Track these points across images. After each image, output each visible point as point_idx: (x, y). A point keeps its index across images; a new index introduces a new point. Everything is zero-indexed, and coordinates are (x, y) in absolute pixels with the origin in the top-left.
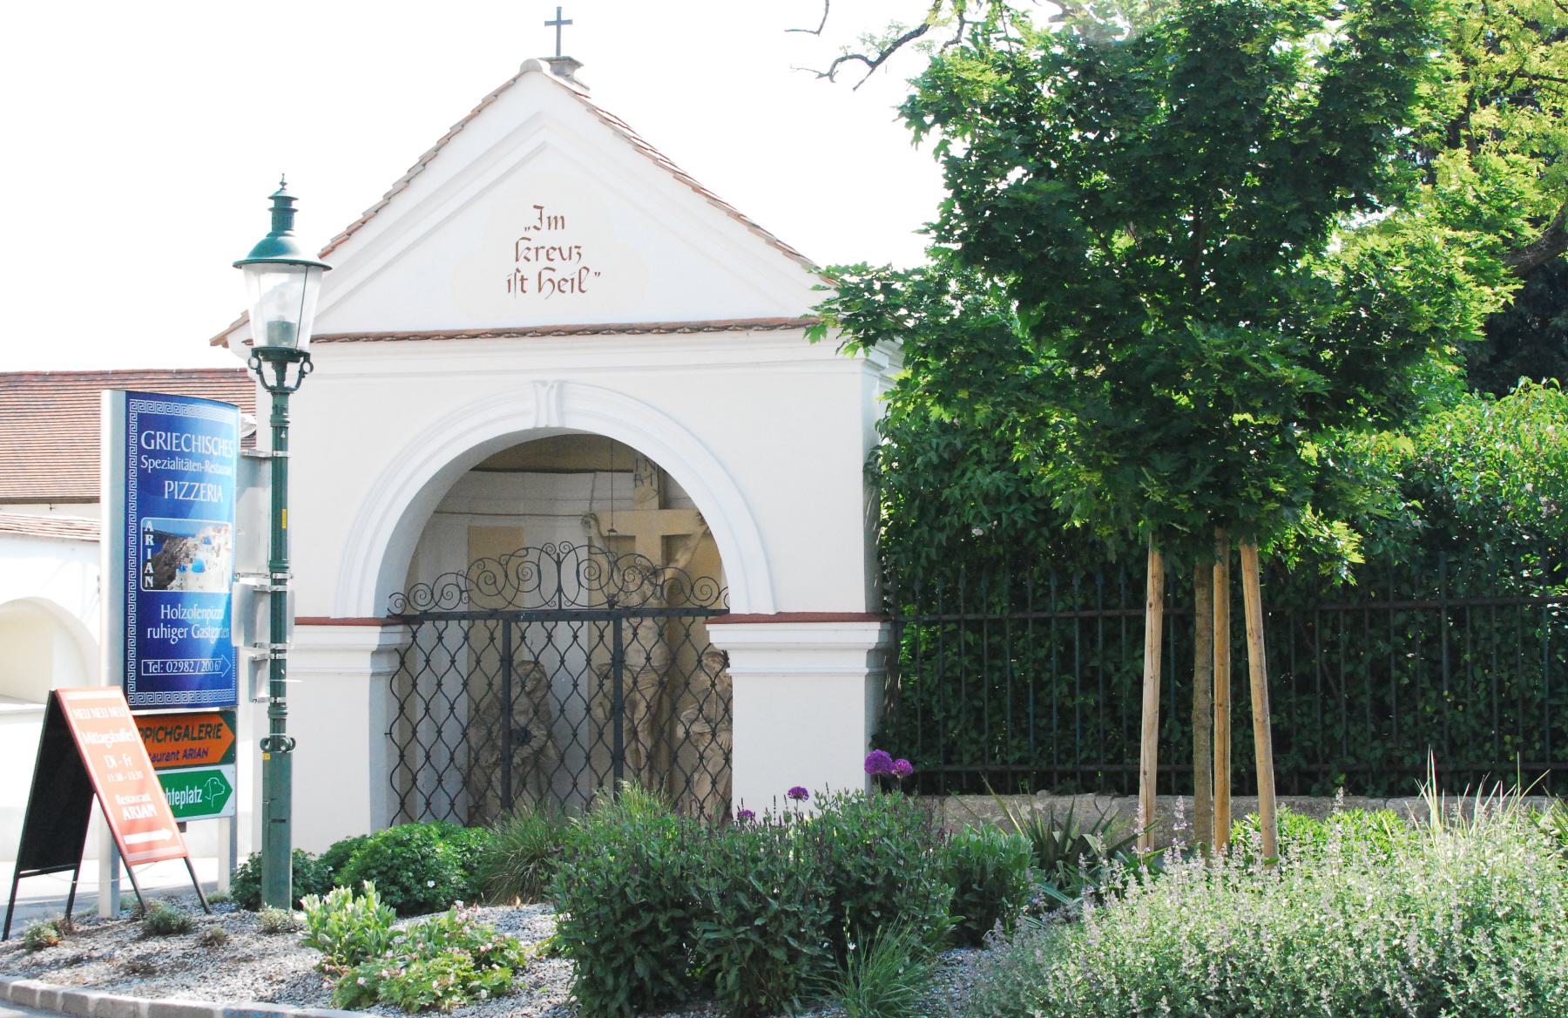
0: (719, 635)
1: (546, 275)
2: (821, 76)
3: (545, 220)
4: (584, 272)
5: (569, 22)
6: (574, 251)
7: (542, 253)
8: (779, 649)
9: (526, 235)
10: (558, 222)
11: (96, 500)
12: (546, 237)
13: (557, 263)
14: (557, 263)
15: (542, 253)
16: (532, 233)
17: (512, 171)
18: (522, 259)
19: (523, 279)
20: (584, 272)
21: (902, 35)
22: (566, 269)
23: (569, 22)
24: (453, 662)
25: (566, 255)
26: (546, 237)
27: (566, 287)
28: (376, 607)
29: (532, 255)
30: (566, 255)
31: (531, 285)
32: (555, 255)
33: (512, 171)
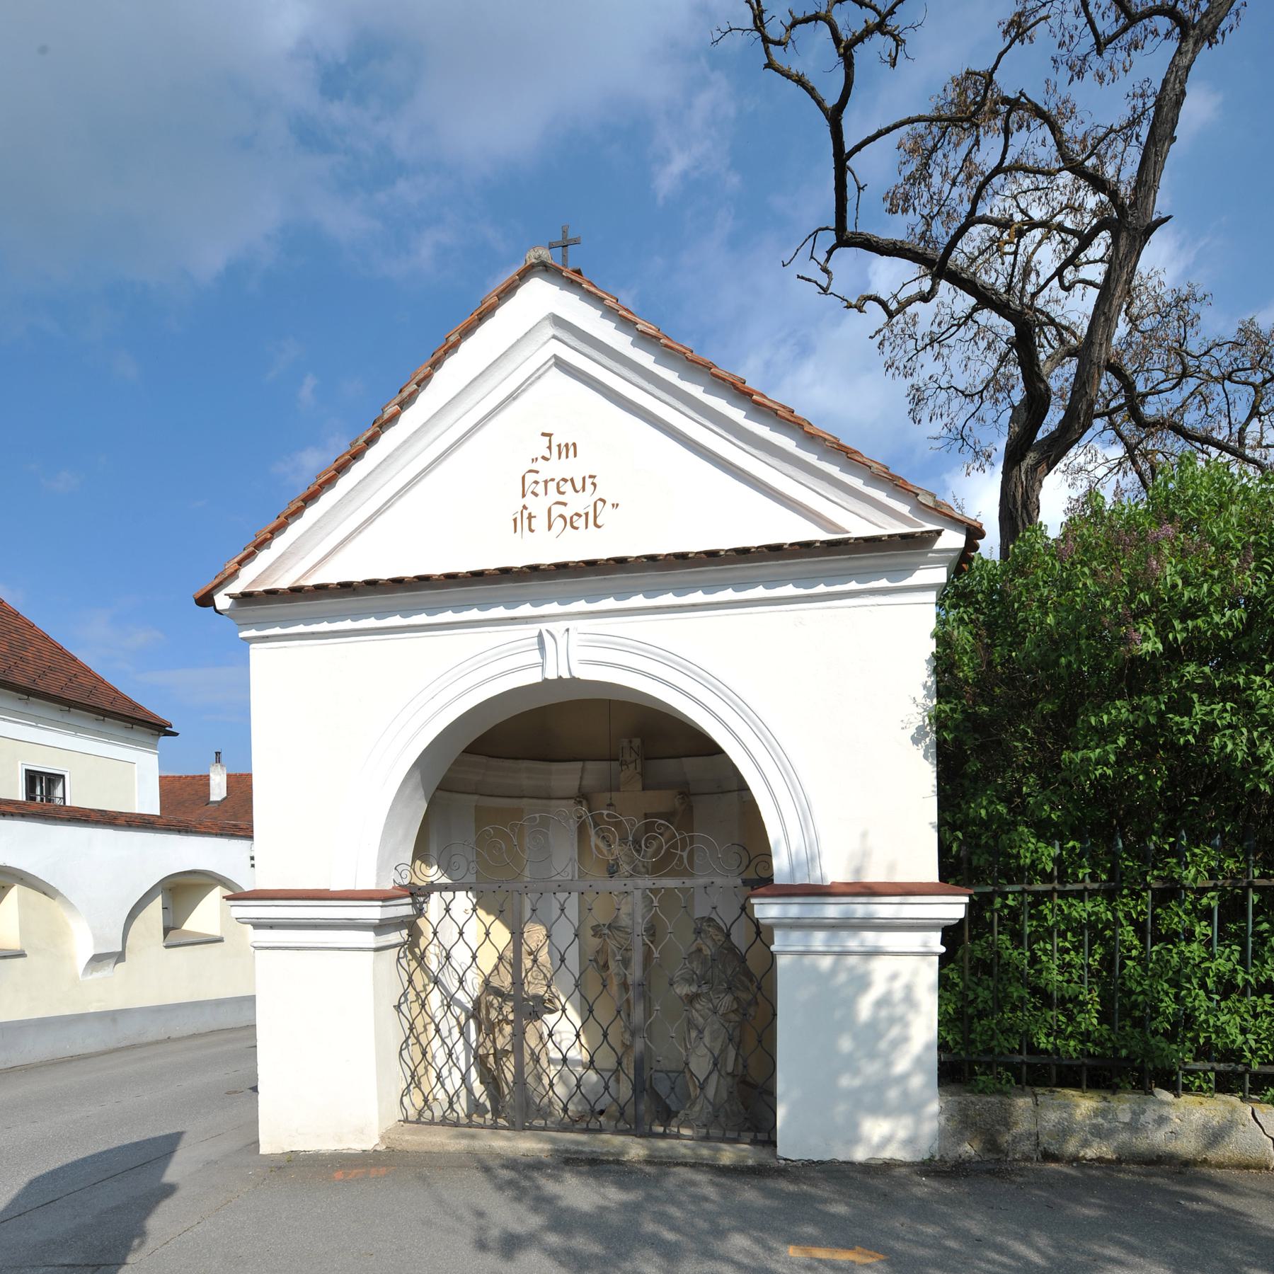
0: (768, 910)
1: (557, 510)
2: (849, 306)
3: (555, 449)
4: (600, 504)
5: (576, 242)
6: (588, 481)
7: (552, 486)
8: (494, 678)
9: (534, 467)
10: (568, 449)
11: (540, 635)
12: (557, 468)
13: (570, 496)
14: (570, 496)
15: (552, 486)
16: (540, 465)
17: (512, 397)
18: (529, 495)
19: (530, 517)
20: (600, 504)
21: (956, 225)
22: (579, 503)
23: (576, 242)
24: (461, 934)
25: (579, 486)
26: (557, 468)
27: (580, 522)
28: (380, 869)
29: (540, 489)
30: (579, 486)
31: (540, 523)
32: (567, 487)
33: (512, 397)
